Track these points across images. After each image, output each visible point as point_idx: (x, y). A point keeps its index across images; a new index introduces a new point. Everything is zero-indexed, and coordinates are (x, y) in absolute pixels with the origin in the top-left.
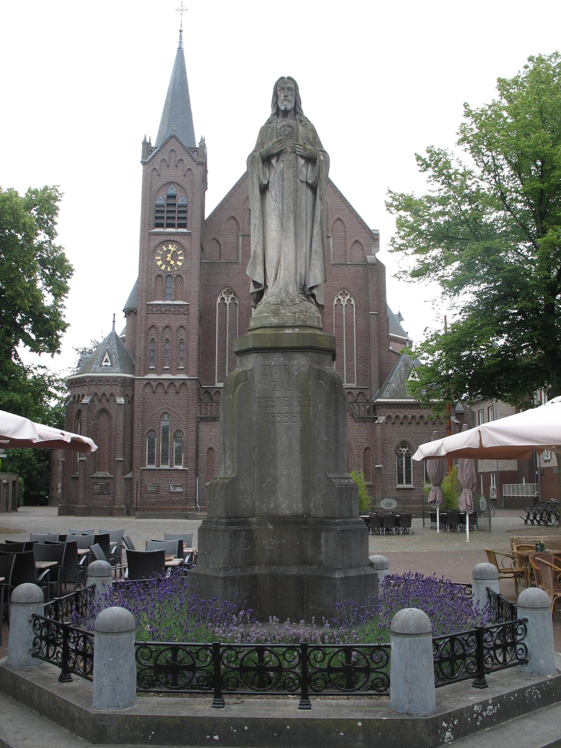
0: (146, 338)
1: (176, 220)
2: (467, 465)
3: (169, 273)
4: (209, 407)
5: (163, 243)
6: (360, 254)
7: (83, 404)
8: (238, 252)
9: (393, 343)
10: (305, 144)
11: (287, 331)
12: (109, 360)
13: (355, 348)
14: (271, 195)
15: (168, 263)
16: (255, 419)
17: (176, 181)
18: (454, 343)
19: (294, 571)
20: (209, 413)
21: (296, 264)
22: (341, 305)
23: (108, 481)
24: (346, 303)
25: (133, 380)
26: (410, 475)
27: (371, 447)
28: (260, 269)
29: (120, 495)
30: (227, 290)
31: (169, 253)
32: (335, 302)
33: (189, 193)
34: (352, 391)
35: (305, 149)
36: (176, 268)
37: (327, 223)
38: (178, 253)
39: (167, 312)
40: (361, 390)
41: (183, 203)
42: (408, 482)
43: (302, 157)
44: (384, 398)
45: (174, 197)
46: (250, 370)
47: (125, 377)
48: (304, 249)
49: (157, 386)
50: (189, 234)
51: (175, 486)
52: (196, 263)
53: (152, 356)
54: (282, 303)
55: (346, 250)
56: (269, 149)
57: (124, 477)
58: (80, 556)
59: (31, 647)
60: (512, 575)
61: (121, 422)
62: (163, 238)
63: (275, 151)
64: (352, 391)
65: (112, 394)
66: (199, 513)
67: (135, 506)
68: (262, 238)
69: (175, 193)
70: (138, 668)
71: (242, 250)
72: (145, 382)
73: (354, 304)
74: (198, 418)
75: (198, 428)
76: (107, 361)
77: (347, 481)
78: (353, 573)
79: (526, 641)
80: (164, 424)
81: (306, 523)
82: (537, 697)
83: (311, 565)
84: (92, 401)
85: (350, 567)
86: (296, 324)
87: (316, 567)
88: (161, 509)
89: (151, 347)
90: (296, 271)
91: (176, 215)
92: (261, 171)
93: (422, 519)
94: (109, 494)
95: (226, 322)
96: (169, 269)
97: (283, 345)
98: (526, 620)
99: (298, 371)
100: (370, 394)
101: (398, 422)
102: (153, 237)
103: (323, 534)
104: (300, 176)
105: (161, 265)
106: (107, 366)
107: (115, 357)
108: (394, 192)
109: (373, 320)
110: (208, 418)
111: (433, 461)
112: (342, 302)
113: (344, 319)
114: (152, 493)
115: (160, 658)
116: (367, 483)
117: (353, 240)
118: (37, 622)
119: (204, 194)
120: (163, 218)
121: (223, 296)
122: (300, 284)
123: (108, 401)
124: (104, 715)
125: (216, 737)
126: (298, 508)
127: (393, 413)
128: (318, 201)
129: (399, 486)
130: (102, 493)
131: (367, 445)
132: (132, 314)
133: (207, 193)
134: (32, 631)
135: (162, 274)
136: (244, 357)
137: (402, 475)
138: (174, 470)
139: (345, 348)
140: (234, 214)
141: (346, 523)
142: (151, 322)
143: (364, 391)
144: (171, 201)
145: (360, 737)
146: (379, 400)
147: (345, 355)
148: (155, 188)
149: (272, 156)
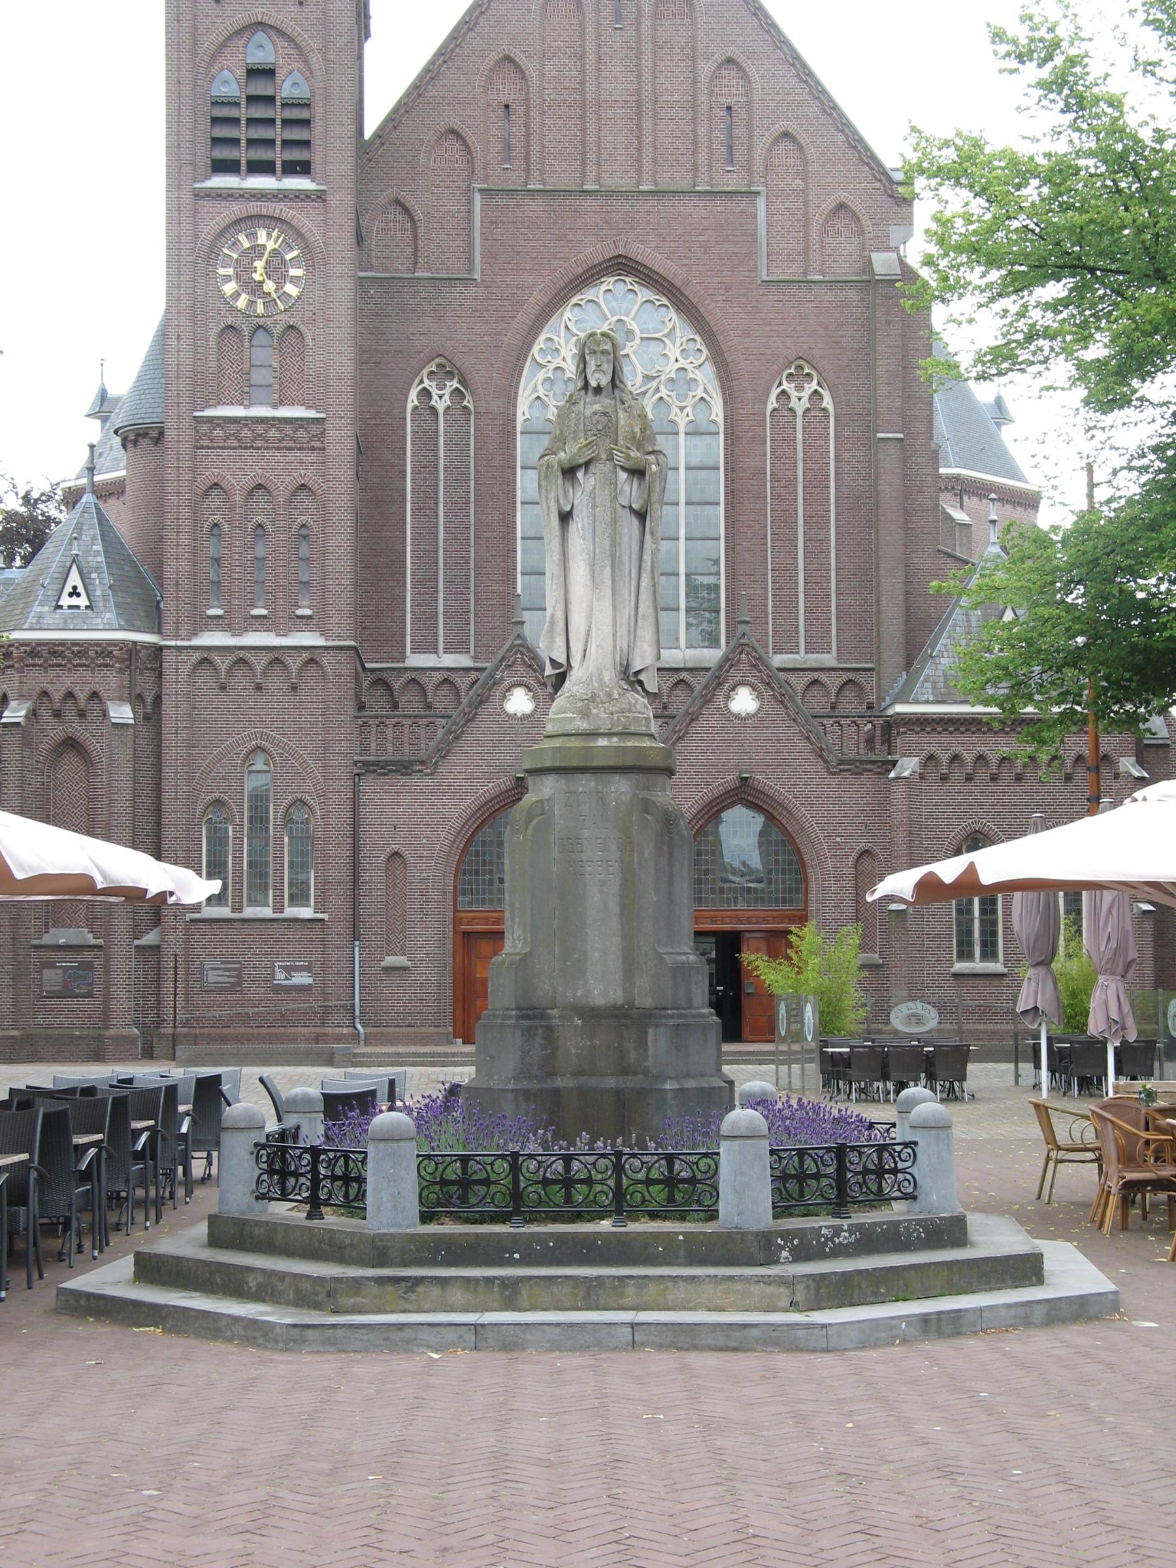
0: (196, 519)
1: (278, 149)
2: (1110, 912)
3: (261, 321)
4: (389, 732)
5: (239, 223)
6: (850, 248)
7: (5, 725)
8: (471, 246)
9: (975, 499)
10: (628, 448)
11: (602, 742)
12: (81, 589)
13: (833, 544)
14: (578, 526)
15: (255, 289)
16: (555, 869)
17: (271, 22)
18: (1084, 570)
19: (610, 1082)
20: (390, 749)
21: (614, 635)
22: (791, 410)
23: (87, 956)
24: (805, 404)
25: (158, 650)
26: (994, 934)
27: (877, 850)
28: (560, 641)
29: (123, 1000)
30: (439, 366)
31: (260, 257)
32: (772, 403)
33: (316, 60)
34: (823, 677)
35: (628, 458)
36: (281, 306)
37: (750, 148)
38: (288, 257)
39: (258, 443)
40: (850, 675)
41: (296, 93)
42: (989, 953)
43: (623, 468)
44: (917, 702)
45: (268, 73)
46: (548, 800)
47: (135, 643)
48: (627, 611)
49: (230, 669)
50: (320, 196)
51: (289, 970)
52: (343, 293)
53: (213, 576)
54: (593, 698)
55: (807, 235)
56: (573, 458)
57: (136, 942)
58: (137, 1133)
59: (254, 1187)
60: (1089, 1155)
61: (123, 778)
62: (237, 209)
63: (582, 461)
64: (823, 677)
65: (95, 695)
66: (362, 1049)
67: (170, 1031)
68: (563, 593)
69: (272, 60)
70: (420, 1184)
71: (484, 239)
72: (197, 655)
73: (471, 407)
74: (355, 763)
75: (356, 794)
76: (74, 593)
77: (684, 957)
78: (691, 1084)
79: (914, 1171)
80: (252, 783)
81: (627, 1016)
82: (919, 1236)
83: (635, 1074)
84: (33, 714)
85: (688, 1076)
86: (615, 730)
87: (641, 1076)
88: (248, 1039)
89: (211, 549)
90: (615, 647)
91: (278, 133)
92: (561, 492)
93: (1012, 1065)
94: (89, 995)
95: (436, 467)
96: (260, 309)
97: (595, 764)
98: (915, 1143)
99: (616, 800)
100: (879, 685)
101: (958, 774)
102: (207, 204)
103: (651, 1031)
104: (620, 499)
105: (236, 295)
106: (78, 607)
107: (101, 582)
108: (927, 133)
109: (890, 461)
110: (387, 763)
111: (1032, 895)
112: (794, 403)
113: (800, 455)
114: (220, 989)
115: (447, 1172)
116: (865, 957)
117: (829, 204)
118: (262, 1152)
119: (360, 57)
120: (235, 142)
121: (427, 383)
122: (621, 665)
123: (82, 714)
124: (385, 1234)
125: (517, 1256)
126: (616, 996)
127: (942, 745)
128: (648, 537)
129: (960, 966)
130: (66, 993)
131: (862, 846)
132: (144, 442)
133: (369, 47)
134: (254, 1165)
135: (239, 322)
136: (538, 779)
137: (970, 933)
138: (285, 920)
139: (801, 544)
140: (455, 123)
141: (682, 1016)
142: (208, 475)
143: (860, 678)
144: (261, 88)
145: (682, 1252)
146: (900, 708)
147: (801, 566)
148: (208, 43)
149: (579, 467)
